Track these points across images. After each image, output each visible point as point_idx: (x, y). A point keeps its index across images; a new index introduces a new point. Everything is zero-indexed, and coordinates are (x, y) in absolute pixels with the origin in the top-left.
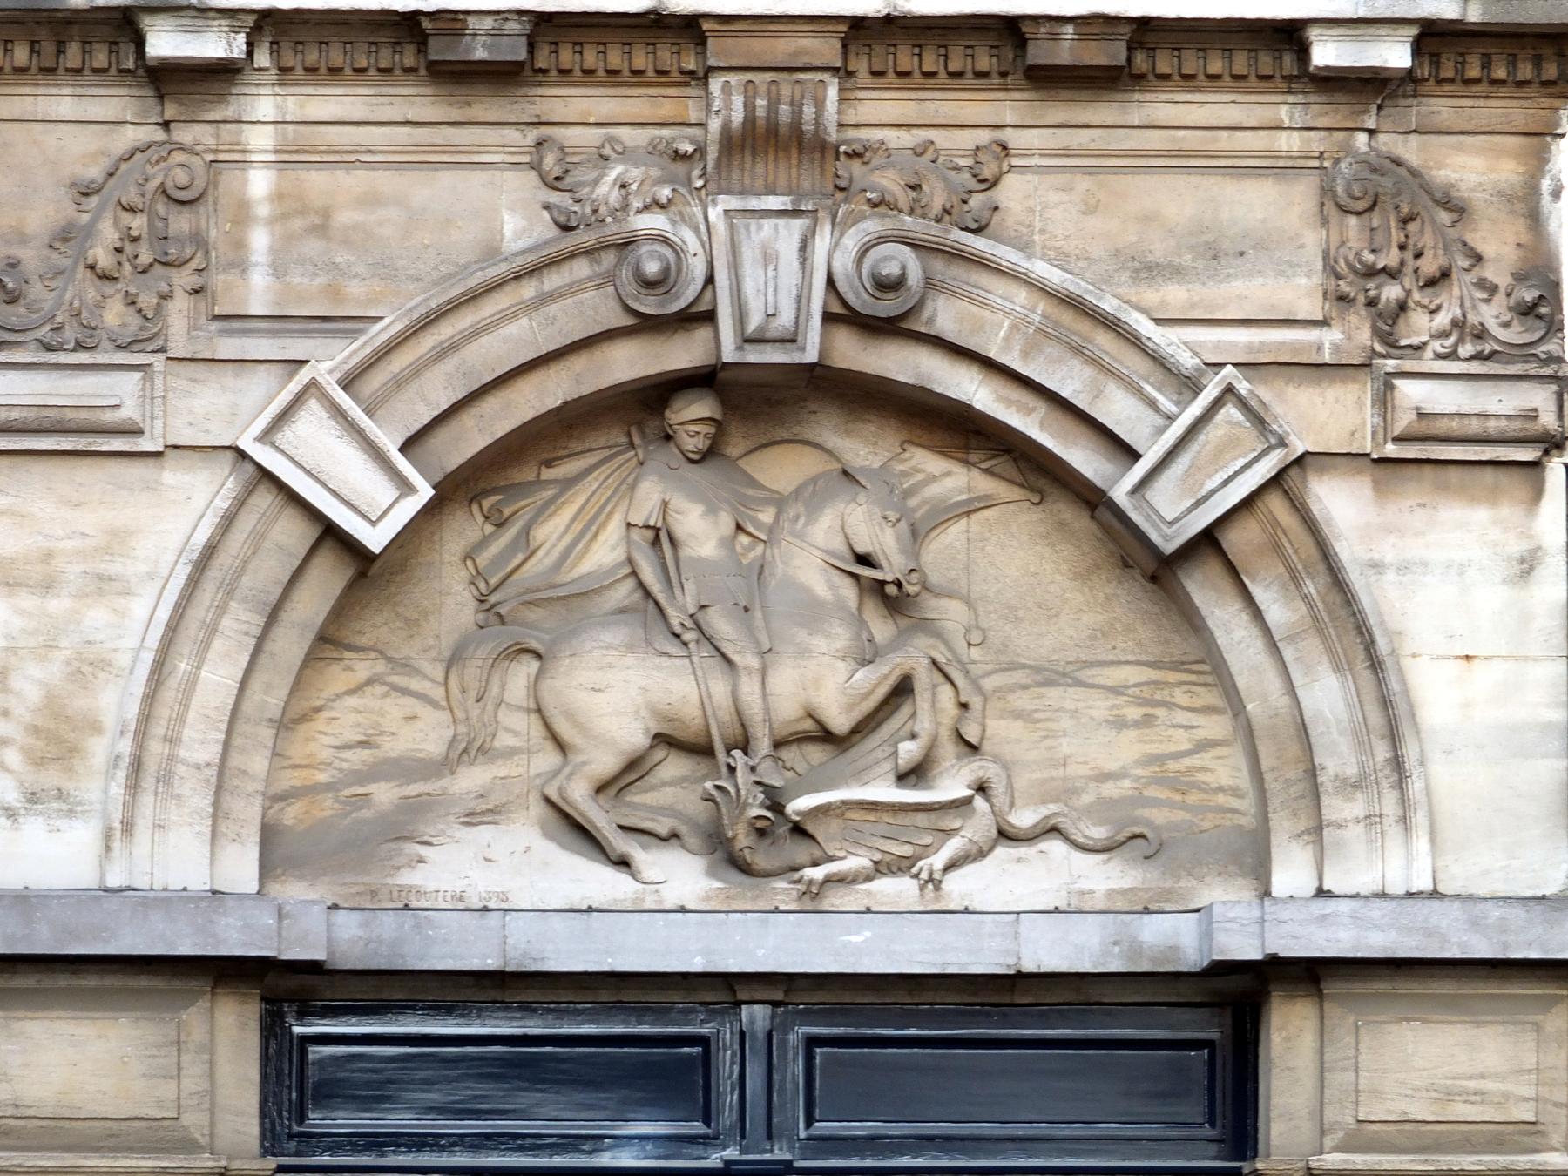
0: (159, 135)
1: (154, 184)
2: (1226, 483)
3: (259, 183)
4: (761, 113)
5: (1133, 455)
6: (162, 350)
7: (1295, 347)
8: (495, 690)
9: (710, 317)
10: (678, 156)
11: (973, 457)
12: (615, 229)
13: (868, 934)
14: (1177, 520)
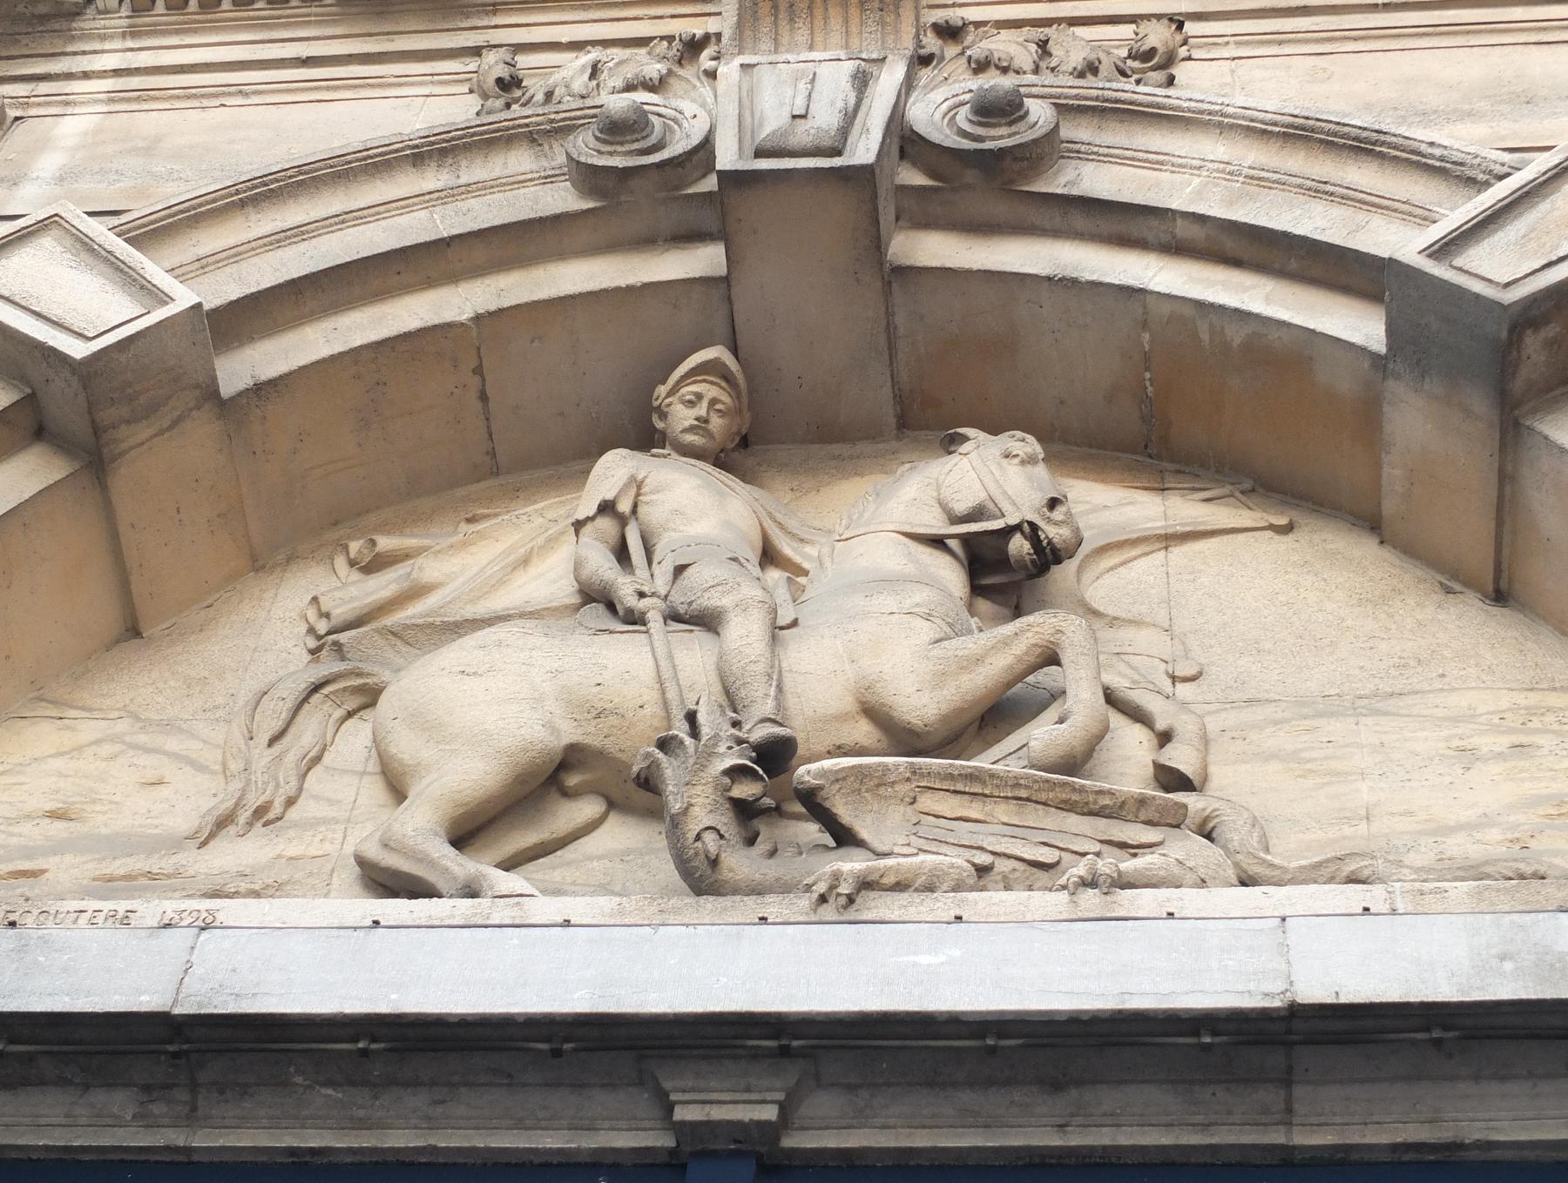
13: (957, 953)
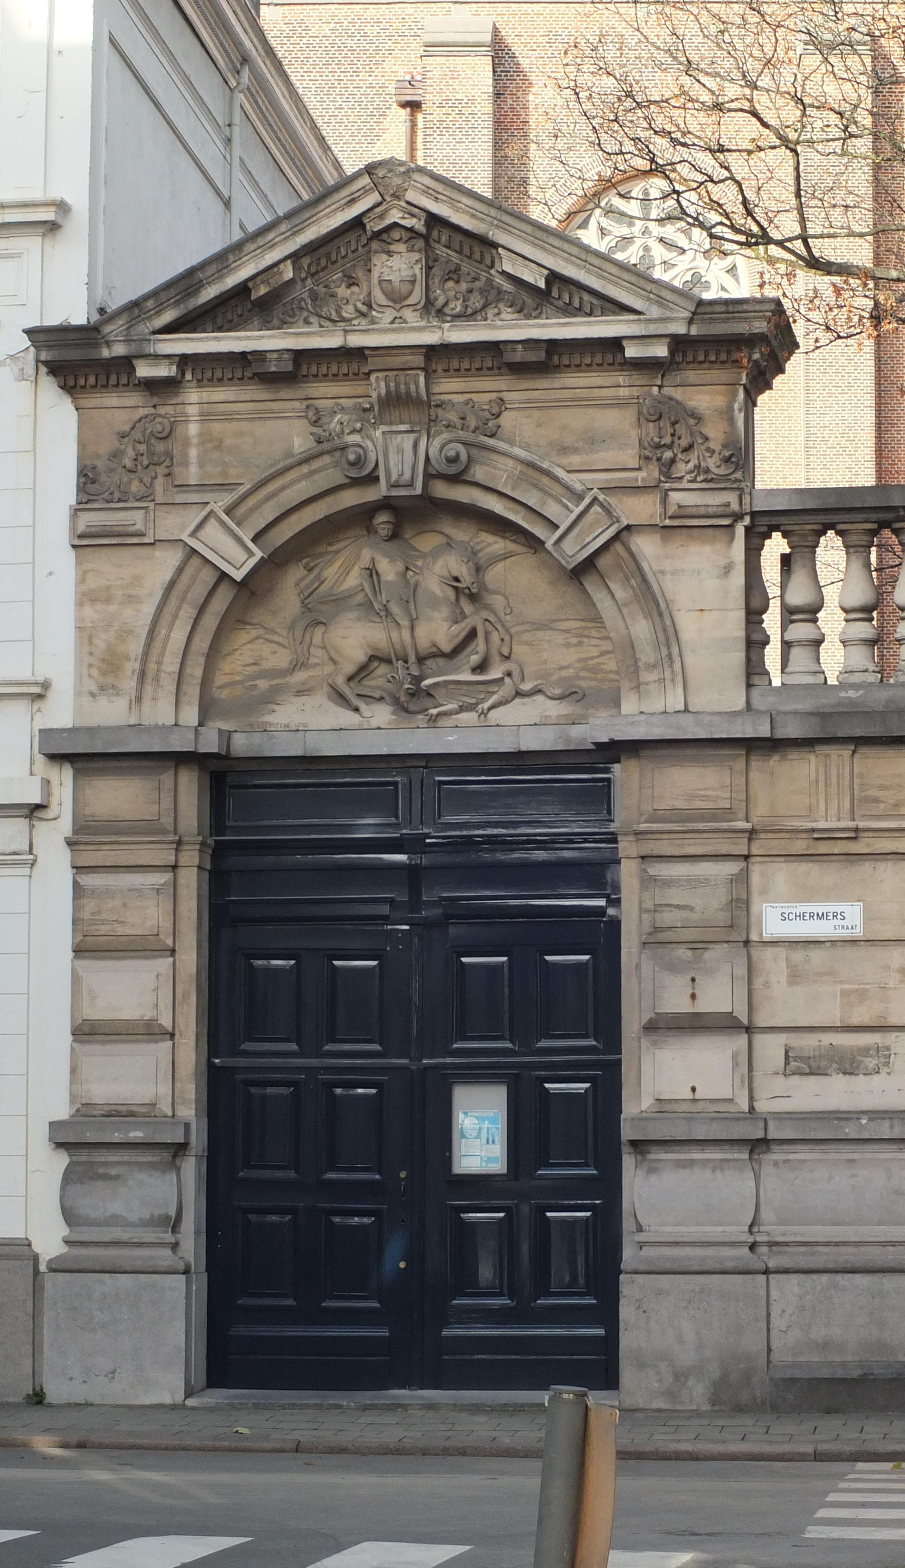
0: (153, 411)
1: (149, 431)
2: (594, 539)
3: (193, 429)
4: (393, 389)
5: (557, 527)
6: (153, 500)
7: (625, 479)
8: (307, 638)
9: (377, 479)
10: (365, 410)
11: (507, 535)
12: (338, 442)
14: (574, 555)
